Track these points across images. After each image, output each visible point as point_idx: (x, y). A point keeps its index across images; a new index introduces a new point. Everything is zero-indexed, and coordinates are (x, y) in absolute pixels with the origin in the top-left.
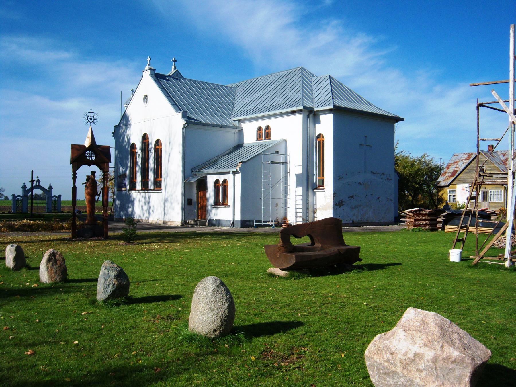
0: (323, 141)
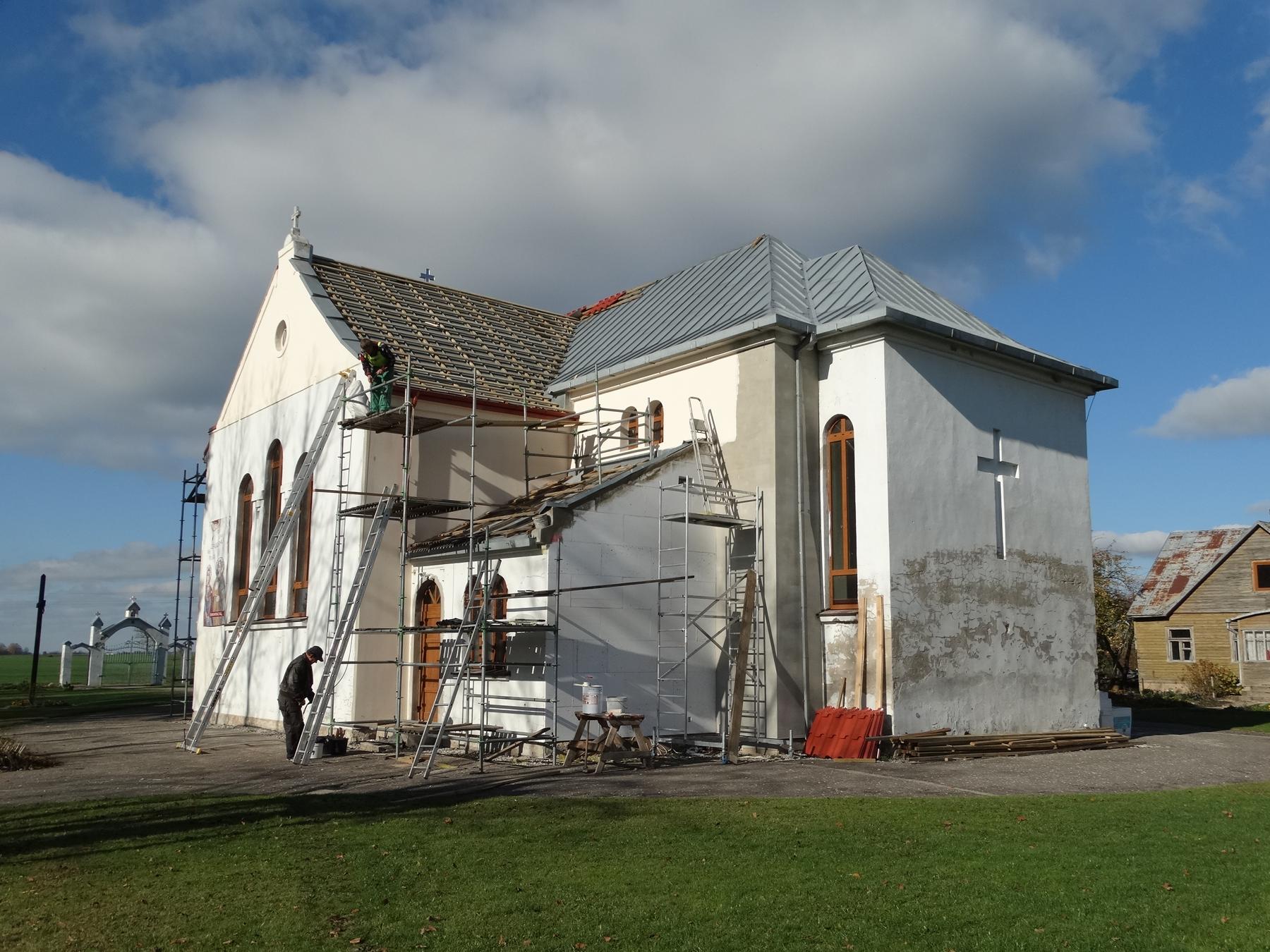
0: (852, 441)
